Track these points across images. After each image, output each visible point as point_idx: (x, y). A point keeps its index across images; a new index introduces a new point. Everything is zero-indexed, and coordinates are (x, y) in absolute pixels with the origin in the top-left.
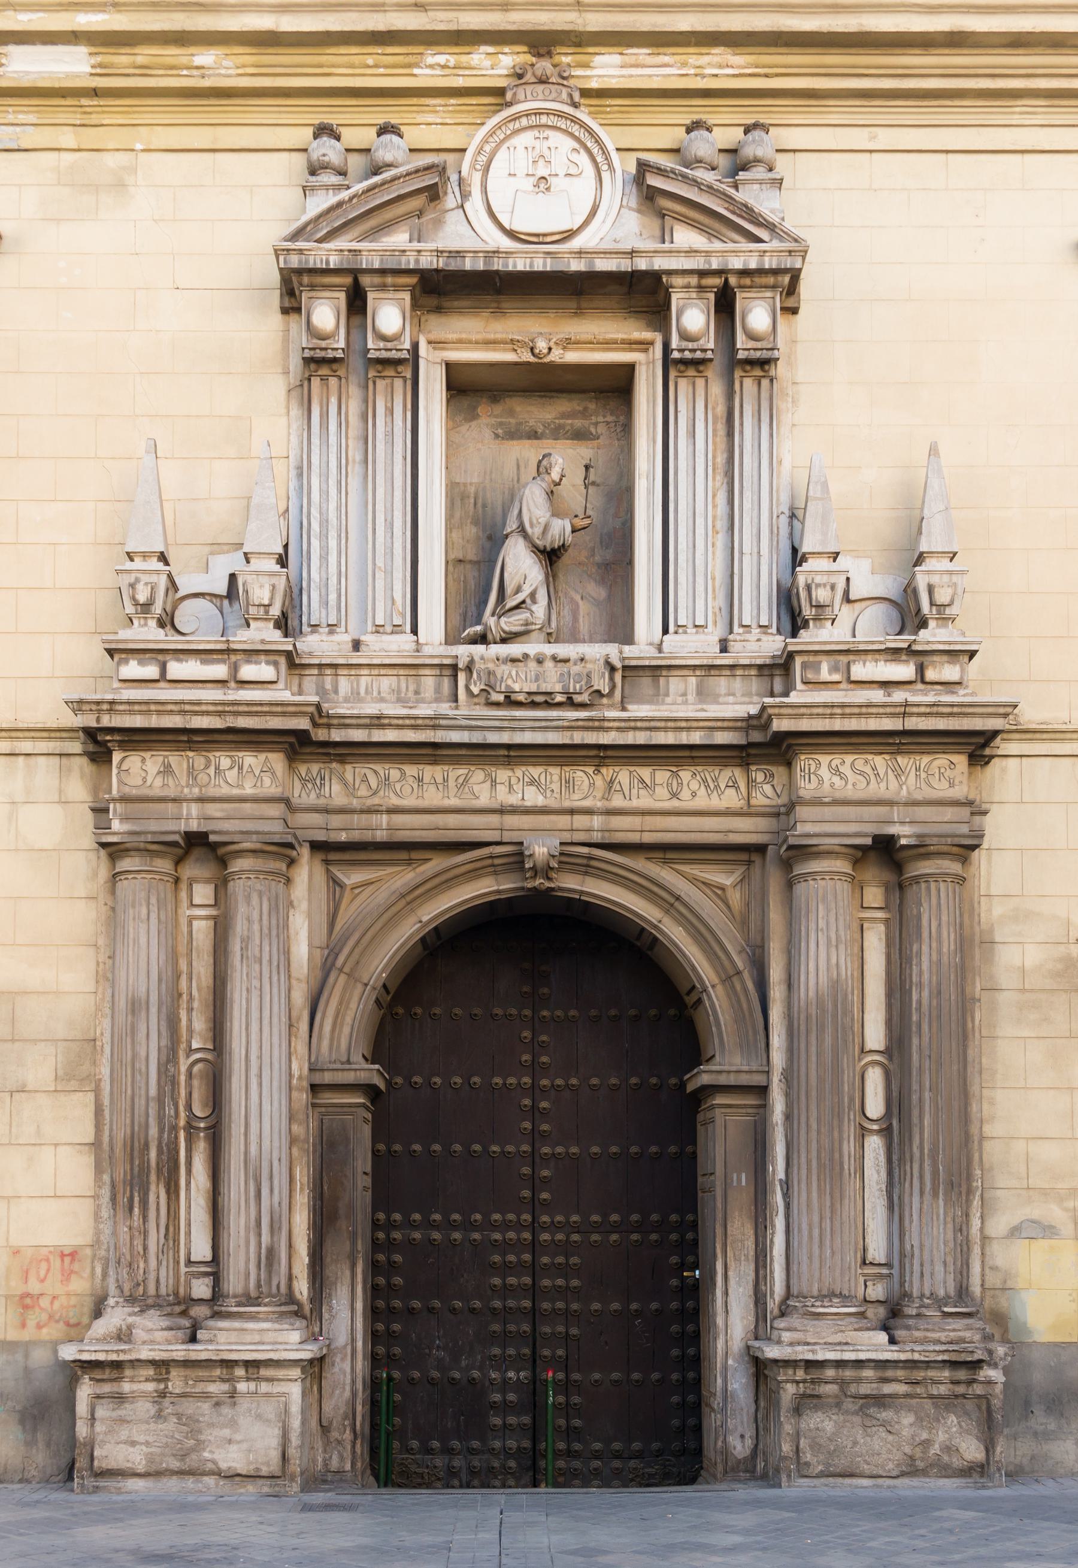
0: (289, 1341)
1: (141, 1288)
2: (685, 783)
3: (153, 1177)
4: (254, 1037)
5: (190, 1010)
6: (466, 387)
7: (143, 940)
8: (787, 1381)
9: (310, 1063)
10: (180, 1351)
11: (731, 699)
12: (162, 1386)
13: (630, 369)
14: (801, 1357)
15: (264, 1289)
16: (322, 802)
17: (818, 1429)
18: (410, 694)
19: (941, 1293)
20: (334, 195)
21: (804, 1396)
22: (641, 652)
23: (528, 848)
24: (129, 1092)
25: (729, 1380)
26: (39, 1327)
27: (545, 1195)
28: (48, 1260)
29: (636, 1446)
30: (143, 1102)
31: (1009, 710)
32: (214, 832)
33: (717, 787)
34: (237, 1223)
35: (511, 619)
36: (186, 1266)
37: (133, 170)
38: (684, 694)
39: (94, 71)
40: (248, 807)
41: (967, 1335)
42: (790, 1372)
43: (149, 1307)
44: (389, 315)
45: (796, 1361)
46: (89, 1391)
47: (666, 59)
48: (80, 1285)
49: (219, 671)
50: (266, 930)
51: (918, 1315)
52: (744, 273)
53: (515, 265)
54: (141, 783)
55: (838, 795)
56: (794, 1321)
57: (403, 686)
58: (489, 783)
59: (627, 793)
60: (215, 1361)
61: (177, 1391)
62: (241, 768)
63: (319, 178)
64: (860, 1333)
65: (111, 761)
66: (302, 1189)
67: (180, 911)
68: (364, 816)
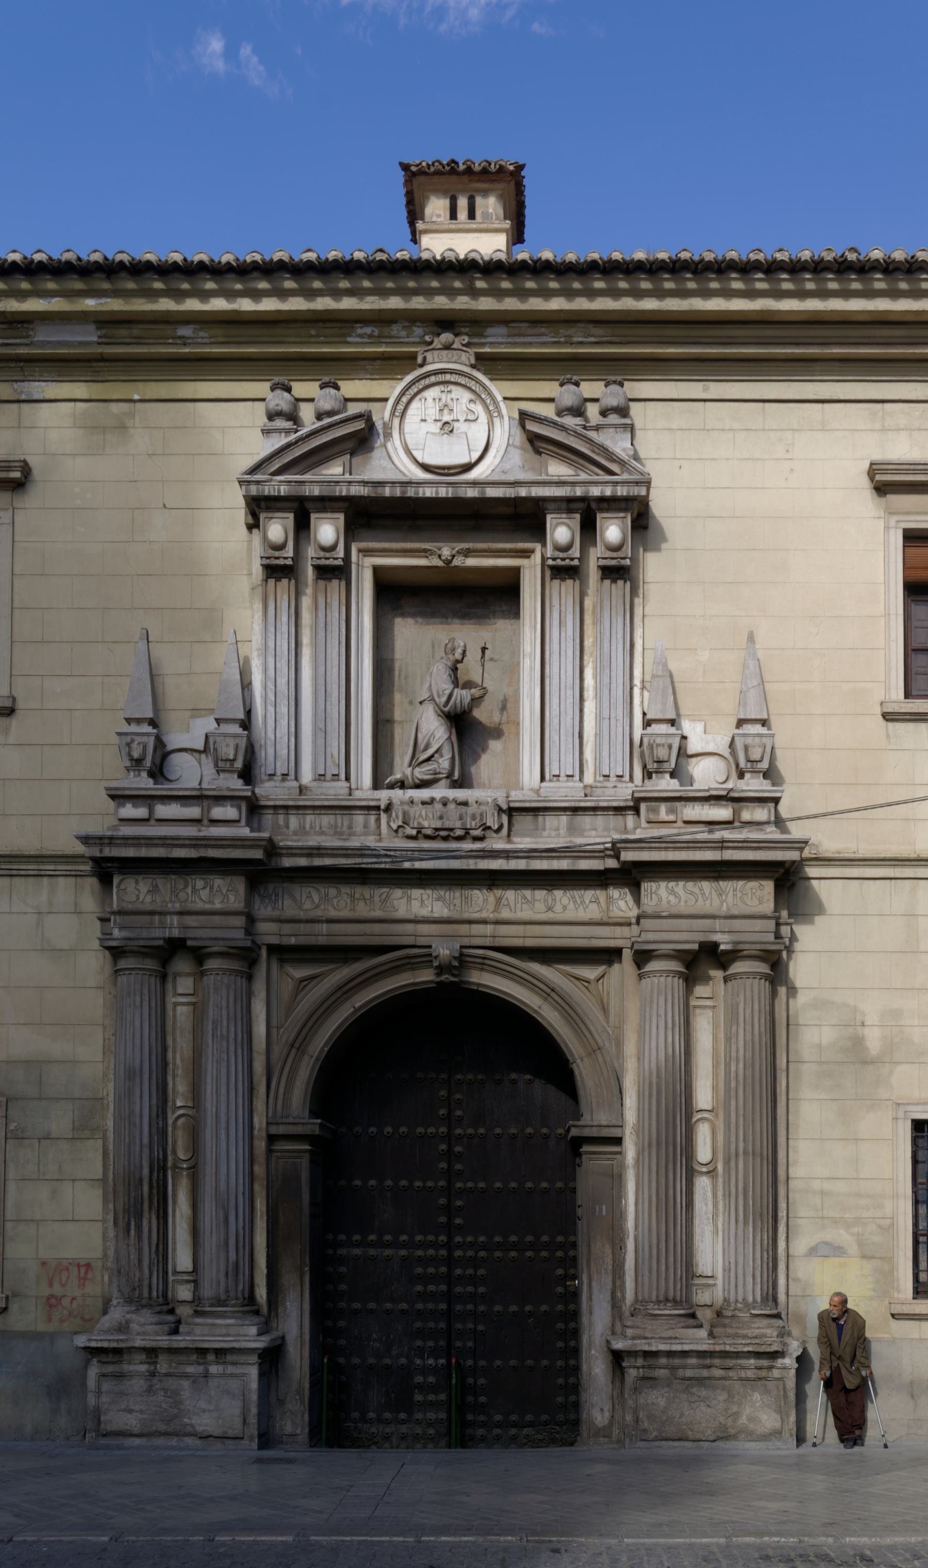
0: (250, 1336)
1: (137, 1293)
2: (558, 899)
3: (146, 1206)
4: (223, 1098)
5: (174, 1077)
6: (394, 593)
7: (138, 1022)
8: (630, 1367)
9: (267, 1117)
10: (164, 1341)
11: (593, 833)
12: (152, 1368)
13: (517, 571)
14: (638, 1348)
15: (232, 1294)
16: (276, 913)
17: (653, 1404)
18: (345, 829)
19: (750, 1299)
20: (286, 436)
21: (644, 1378)
22: (524, 796)
23: (435, 950)
24: (127, 1140)
25: (596, 1368)
26: (62, 1321)
27: (458, 1221)
28: (67, 1269)
29: (529, 1418)
30: (138, 1148)
31: (803, 845)
32: (191, 939)
33: (583, 902)
34: (210, 1242)
35: (423, 770)
36: (173, 1275)
37: (132, 415)
38: (558, 829)
39: (100, 340)
40: (217, 918)
41: (768, 1331)
42: (633, 1360)
43: (144, 1306)
44: (327, 530)
45: (636, 1352)
46: (97, 1371)
47: (543, 330)
48: (94, 1289)
49: (194, 812)
50: (232, 1015)
51: (733, 1316)
52: (602, 500)
53: (424, 493)
54: (135, 899)
55: (674, 911)
56: (638, 1320)
57: (339, 821)
58: (405, 899)
59: (513, 906)
60: (192, 1349)
61: (163, 1371)
62: (212, 888)
63: (274, 423)
64: (685, 1330)
65: (112, 882)
66: (261, 1216)
67: (167, 999)
68: (309, 925)
